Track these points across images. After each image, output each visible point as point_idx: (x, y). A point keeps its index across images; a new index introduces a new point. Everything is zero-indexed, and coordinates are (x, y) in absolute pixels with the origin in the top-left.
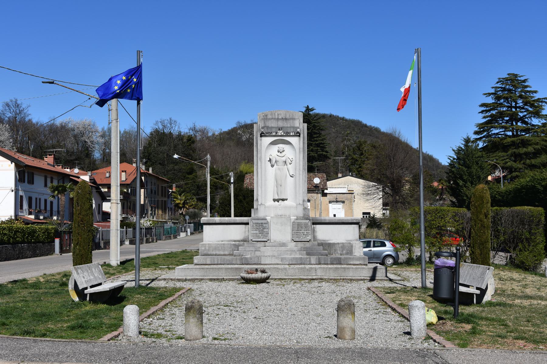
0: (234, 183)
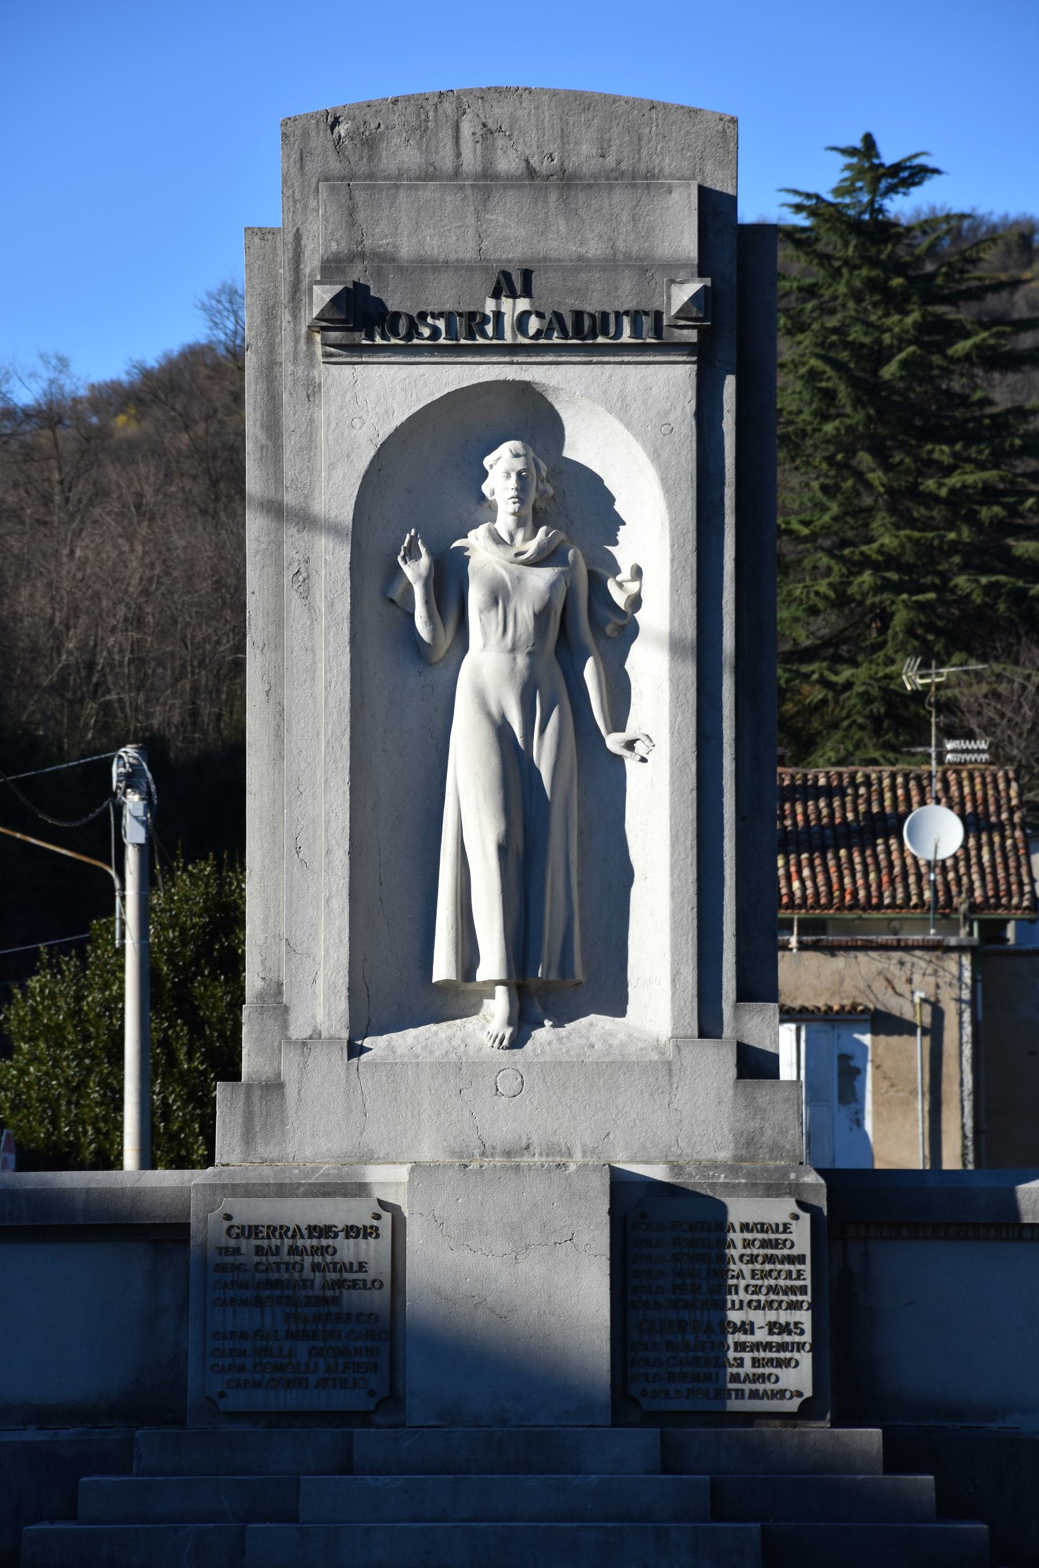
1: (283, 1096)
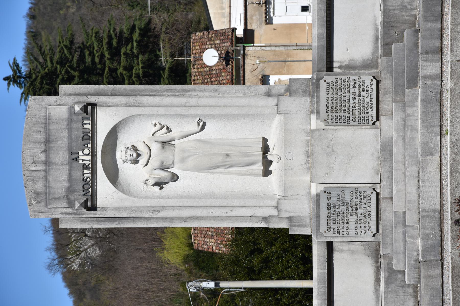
0: (215, 279)
1: (293, 217)
